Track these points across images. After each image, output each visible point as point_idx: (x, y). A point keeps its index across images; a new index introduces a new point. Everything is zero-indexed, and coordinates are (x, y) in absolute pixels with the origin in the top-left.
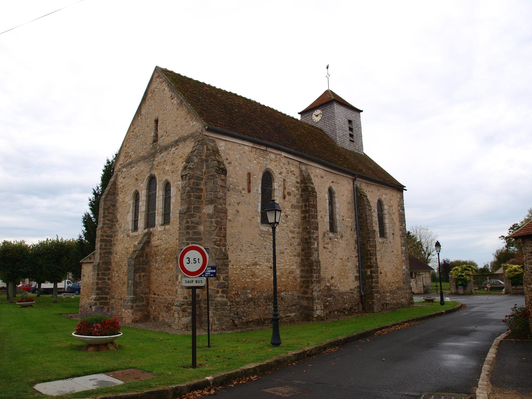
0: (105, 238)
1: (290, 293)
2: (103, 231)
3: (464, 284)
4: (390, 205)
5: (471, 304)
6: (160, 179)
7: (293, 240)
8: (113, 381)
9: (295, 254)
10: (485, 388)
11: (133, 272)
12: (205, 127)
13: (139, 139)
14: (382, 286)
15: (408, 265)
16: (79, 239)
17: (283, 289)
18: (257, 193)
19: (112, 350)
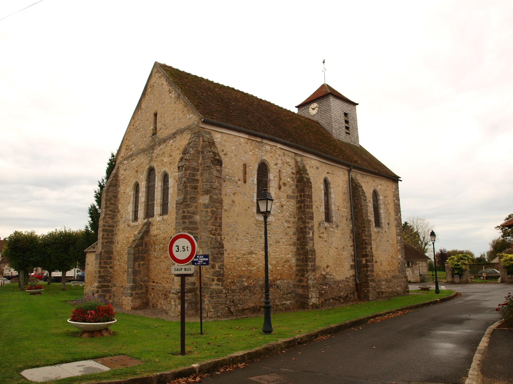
0: (107, 228)
1: (285, 281)
2: (105, 221)
3: (460, 273)
4: (386, 196)
5: (466, 293)
6: (159, 171)
7: (288, 230)
8: (100, 367)
9: (290, 243)
10: (475, 378)
11: (133, 261)
12: (201, 119)
13: (139, 132)
14: (377, 275)
15: (404, 254)
16: (86, 230)
17: (279, 277)
18: (253, 184)
19: (106, 336)
